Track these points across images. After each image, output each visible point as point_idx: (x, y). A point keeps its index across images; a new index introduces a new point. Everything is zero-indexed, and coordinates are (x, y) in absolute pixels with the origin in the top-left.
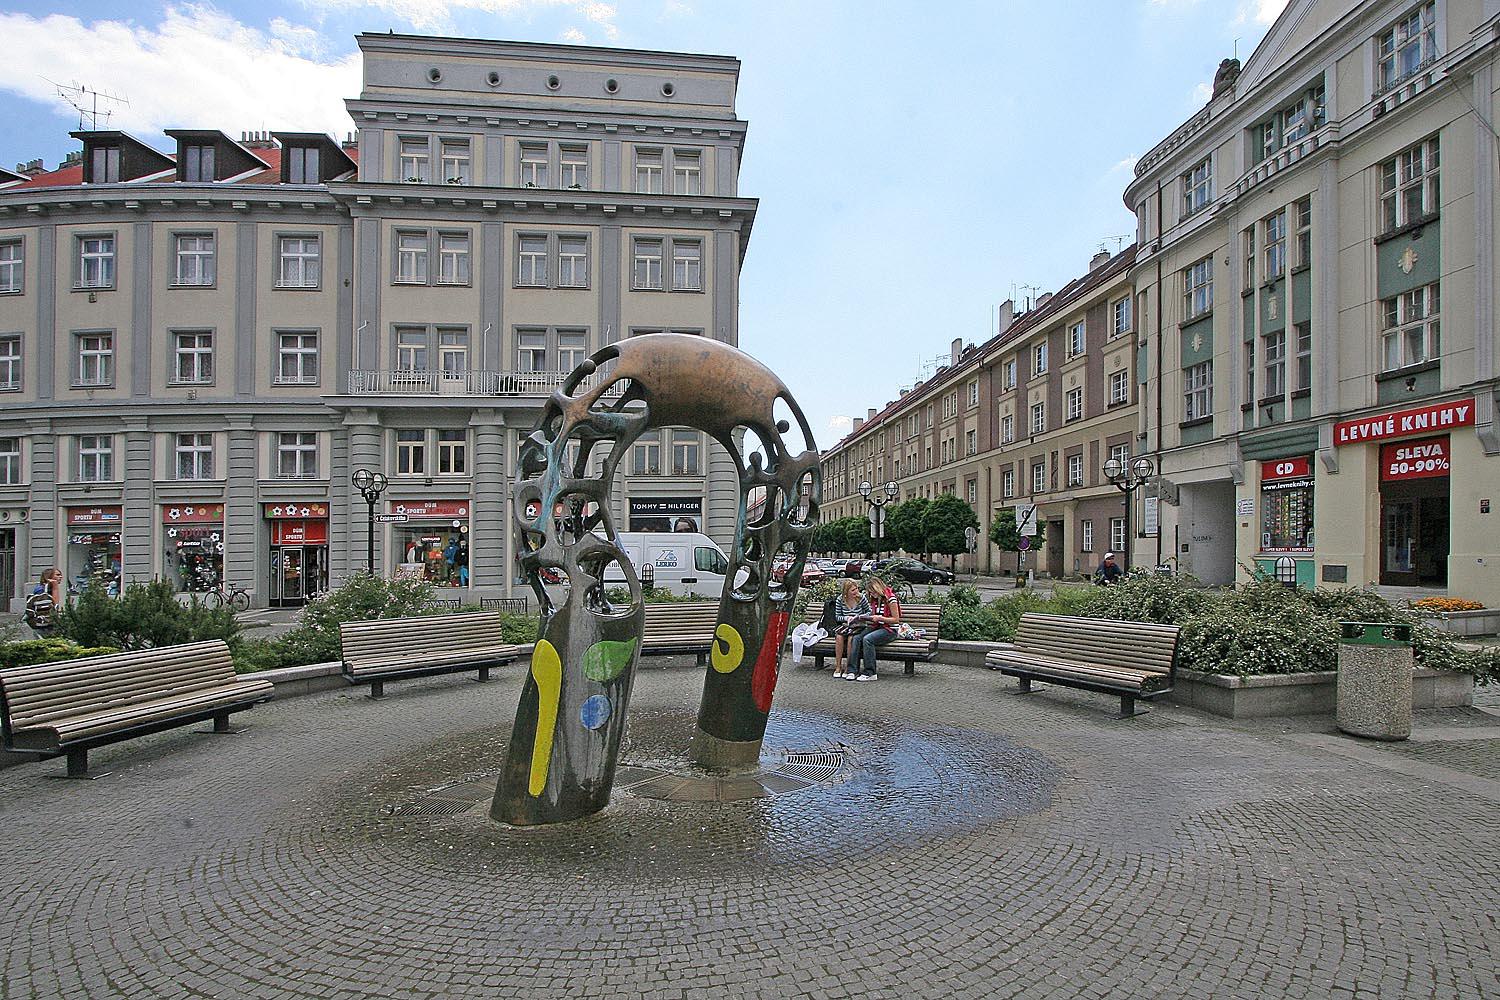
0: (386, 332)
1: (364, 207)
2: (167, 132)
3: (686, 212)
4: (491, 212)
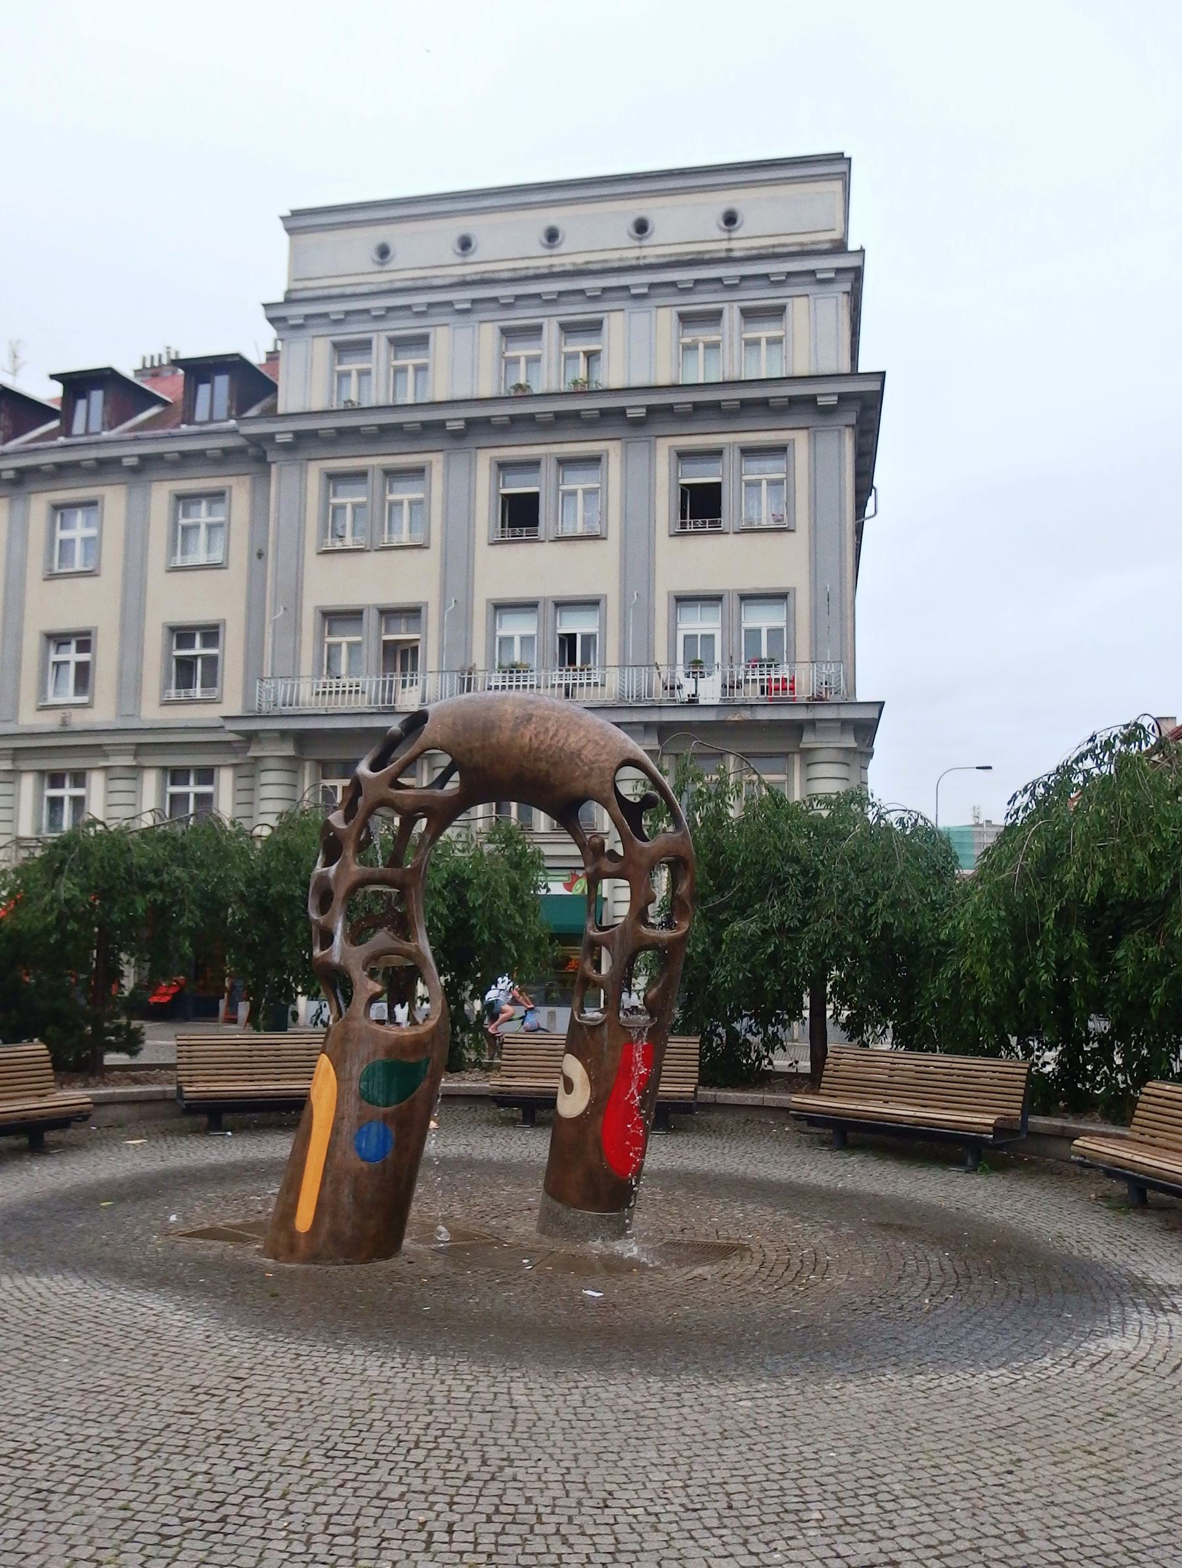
0: (309, 620)
1: (287, 448)
2: (53, 377)
3: (715, 407)
4: (457, 435)
